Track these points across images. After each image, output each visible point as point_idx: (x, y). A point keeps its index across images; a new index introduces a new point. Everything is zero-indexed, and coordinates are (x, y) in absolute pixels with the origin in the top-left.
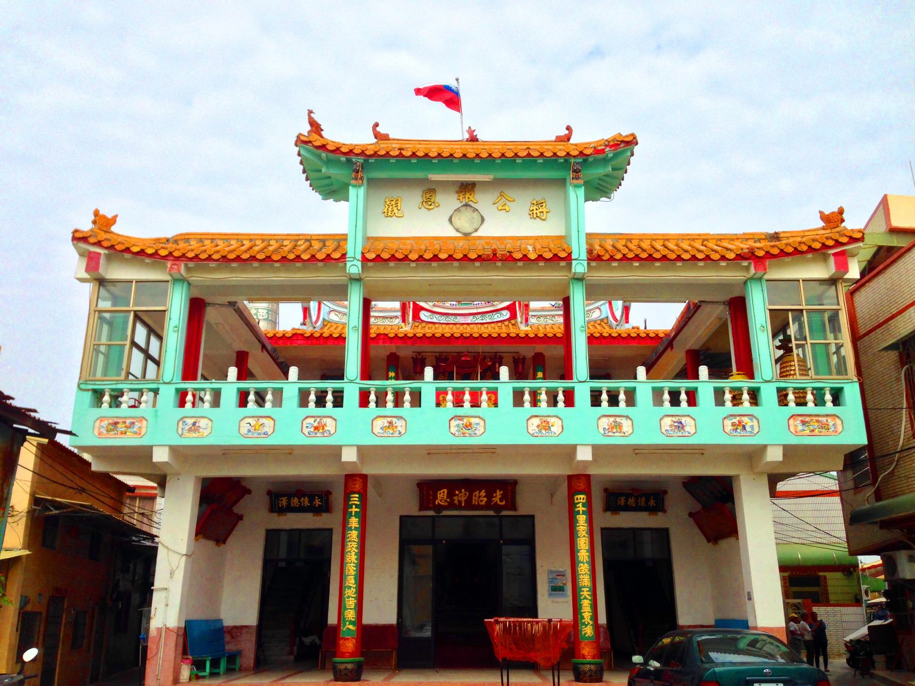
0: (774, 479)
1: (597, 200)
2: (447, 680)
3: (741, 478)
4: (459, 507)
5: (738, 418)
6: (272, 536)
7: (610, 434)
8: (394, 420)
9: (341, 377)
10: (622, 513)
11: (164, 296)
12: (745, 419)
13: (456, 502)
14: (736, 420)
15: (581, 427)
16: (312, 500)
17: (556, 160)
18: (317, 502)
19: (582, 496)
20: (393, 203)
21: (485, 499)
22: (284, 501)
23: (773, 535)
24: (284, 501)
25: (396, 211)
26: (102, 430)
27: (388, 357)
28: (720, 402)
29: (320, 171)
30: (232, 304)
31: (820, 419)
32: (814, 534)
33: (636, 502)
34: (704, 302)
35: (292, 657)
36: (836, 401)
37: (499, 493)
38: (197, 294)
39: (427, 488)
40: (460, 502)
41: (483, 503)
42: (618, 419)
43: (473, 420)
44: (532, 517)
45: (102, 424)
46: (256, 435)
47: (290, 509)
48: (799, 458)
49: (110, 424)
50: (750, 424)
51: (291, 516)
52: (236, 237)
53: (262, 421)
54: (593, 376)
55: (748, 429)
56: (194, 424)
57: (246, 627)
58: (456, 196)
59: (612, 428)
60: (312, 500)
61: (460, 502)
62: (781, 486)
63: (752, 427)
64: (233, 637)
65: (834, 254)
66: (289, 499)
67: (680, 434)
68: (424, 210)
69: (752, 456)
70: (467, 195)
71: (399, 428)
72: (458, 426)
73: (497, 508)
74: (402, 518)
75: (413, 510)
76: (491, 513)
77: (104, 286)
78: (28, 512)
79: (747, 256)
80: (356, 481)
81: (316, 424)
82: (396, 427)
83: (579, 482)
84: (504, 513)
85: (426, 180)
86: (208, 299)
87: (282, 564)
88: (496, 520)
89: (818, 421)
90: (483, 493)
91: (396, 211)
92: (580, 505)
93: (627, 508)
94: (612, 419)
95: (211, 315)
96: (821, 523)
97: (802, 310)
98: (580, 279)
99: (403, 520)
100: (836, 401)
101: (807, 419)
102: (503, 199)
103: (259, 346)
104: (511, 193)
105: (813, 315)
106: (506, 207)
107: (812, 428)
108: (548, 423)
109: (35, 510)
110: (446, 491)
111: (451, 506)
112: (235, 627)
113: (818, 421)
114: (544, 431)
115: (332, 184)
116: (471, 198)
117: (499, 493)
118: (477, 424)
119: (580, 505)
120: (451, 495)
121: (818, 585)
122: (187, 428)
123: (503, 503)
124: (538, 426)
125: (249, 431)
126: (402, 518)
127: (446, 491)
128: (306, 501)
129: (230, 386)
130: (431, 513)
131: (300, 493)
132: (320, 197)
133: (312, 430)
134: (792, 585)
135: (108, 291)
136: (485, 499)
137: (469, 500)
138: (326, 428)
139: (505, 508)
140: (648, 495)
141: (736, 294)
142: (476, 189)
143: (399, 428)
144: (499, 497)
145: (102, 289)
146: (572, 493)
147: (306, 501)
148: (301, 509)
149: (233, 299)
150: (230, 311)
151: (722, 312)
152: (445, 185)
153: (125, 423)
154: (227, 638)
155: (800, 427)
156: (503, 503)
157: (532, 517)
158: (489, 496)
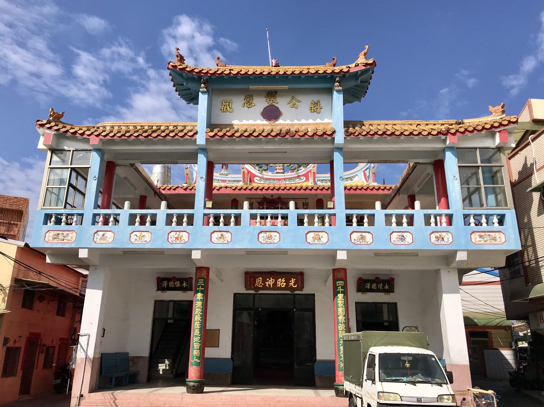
0: (462, 272)
1: (352, 102)
2: (257, 394)
3: (441, 271)
4: (269, 288)
5: (439, 233)
6: (159, 305)
7: (358, 243)
8: (224, 233)
9: (193, 208)
10: (368, 293)
11: (88, 160)
12: (444, 234)
13: (267, 285)
14: (438, 234)
15: (336, 238)
16: (181, 283)
17: (326, 76)
18: (185, 285)
19: (341, 282)
20: (227, 104)
21: (285, 284)
22: (165, 284)
23: (461, 308)
24: (165, 284)
25: (228, 109)
26: (50, 238)
27: (232, 201)
28: (428, 223)
29: (183, 85)
30: (132, 165)
31: (491, 234)
32: (484, 307)
33: (377, 286)
34: (418, 163)
35: (172, 376)
36: (501, 222)
37: (293, 281)
38: (107, 158)
39: (250, 277)
40: (269, 285)
41: (284, 286)
42: (363, 234)
43: (273, 234)
44: (314, 295)
45: (50, 235)
46: (140, 242)
47: (169, 289)
48: (479, 259)
49: (55, 235)
50: (447, 237)
51: (169, 292)
52: (133, 125)
53: (144, 233)
54: (348, 206)
55: (445, 239)
56: (103, 235)
57: (142, 357)
58: (265, 99)
59: (360, 239)
60: (181, 283)
61: (269, 285)
62: (466, 278)
63: (448, 239)
64: (134, 363)
65: (499, 132)
66: (168, 282)
67: (403, 243)
68: (246, 108)
69: (448, 257)
70: (272, 99)
71: (227, 238)
72: (263, 237)
73: (292, 289)
74: (235, 295)
75: (242, 290)
76: (289, 292)
77: (55, 154)
78: (10, 286)
79: (444, 133)
80: (203, 271)
81: (176, 236)
82: (226, 238)
83: (339, 274)
84: (296, 292)
85: (248, 90)
86: (118, 162)
87: (169, 321)
88: (292, 297)
89: (489, 235)
90: (283, 280)
91: (228, 109)
92: (340, 287)
93: (371, 290)
94: (360, 234)
95: (119, 172)
96: (488, 298)
97: (479, 167)
98: (340, 149)
99: (236, 296)
100: (501, 222)
101: (482, 234)
102: (294, 101)
103: (153, 192)
104: (299, 97)
105: (484, 168)
106: (295, 106)
107: (485, 239)
108: (319, 236)
109: (15, 287)
110: (261, 278)
111: (265, 288)
112: (136, 357)
113: (489, 235)
114: (316, 241)
115: (191, 94)
116: (274, 100)
117: (293, 281)
118: (275, 236)
119: (340, 287)
120: (264, 281)
121: (487, 337)
122: (99, 237)
123: (296, 286)
124: (313, 238)
125: (136, 240)
126: (235, 295)
127: (261, 278)
128: (178, 284)
129: (126, 211)
130: (253, 292)
131: (174, 279)
132: (186, 102)
133: (174, 239)
134: (471, 337)
135: (59, 157)
136: (285, 284)
137: (275, 284)
138: (182, 238)
139: (297, 289)
140: (384, 282)
141: (439, 158)
142: (278, 93)
143: (227, 238)
144: (293, 282)
145: (53, 154)
146: (335, 280)
147: (178, 284)
148: (175, 289)
149: (132, 162)
150: (132, 169)
151: (430, 170)
152: (259, 93)
153: (63, 234)
154: (131, 363)
155: (478, 239)
156: (296, 286)
157: (314, 295)
158: (287, 282)
